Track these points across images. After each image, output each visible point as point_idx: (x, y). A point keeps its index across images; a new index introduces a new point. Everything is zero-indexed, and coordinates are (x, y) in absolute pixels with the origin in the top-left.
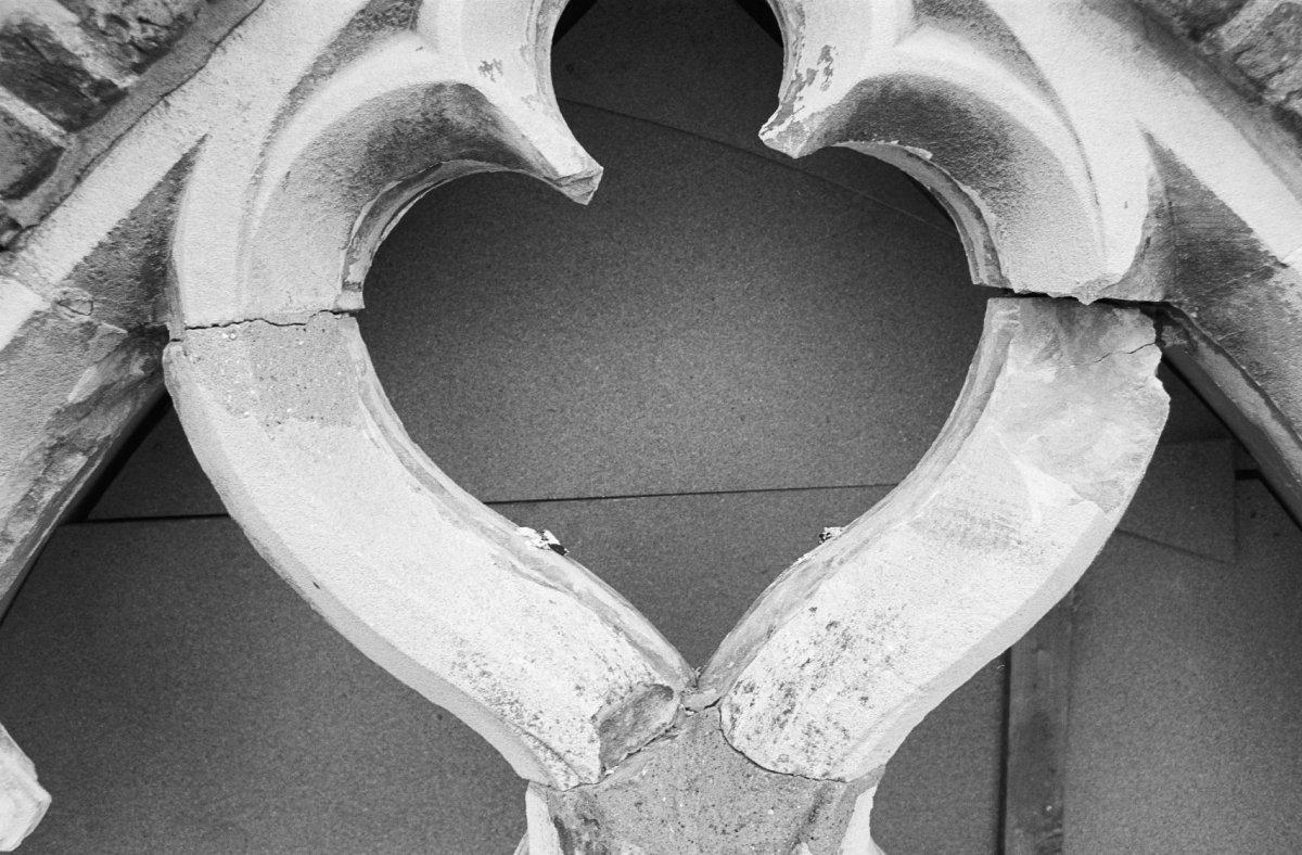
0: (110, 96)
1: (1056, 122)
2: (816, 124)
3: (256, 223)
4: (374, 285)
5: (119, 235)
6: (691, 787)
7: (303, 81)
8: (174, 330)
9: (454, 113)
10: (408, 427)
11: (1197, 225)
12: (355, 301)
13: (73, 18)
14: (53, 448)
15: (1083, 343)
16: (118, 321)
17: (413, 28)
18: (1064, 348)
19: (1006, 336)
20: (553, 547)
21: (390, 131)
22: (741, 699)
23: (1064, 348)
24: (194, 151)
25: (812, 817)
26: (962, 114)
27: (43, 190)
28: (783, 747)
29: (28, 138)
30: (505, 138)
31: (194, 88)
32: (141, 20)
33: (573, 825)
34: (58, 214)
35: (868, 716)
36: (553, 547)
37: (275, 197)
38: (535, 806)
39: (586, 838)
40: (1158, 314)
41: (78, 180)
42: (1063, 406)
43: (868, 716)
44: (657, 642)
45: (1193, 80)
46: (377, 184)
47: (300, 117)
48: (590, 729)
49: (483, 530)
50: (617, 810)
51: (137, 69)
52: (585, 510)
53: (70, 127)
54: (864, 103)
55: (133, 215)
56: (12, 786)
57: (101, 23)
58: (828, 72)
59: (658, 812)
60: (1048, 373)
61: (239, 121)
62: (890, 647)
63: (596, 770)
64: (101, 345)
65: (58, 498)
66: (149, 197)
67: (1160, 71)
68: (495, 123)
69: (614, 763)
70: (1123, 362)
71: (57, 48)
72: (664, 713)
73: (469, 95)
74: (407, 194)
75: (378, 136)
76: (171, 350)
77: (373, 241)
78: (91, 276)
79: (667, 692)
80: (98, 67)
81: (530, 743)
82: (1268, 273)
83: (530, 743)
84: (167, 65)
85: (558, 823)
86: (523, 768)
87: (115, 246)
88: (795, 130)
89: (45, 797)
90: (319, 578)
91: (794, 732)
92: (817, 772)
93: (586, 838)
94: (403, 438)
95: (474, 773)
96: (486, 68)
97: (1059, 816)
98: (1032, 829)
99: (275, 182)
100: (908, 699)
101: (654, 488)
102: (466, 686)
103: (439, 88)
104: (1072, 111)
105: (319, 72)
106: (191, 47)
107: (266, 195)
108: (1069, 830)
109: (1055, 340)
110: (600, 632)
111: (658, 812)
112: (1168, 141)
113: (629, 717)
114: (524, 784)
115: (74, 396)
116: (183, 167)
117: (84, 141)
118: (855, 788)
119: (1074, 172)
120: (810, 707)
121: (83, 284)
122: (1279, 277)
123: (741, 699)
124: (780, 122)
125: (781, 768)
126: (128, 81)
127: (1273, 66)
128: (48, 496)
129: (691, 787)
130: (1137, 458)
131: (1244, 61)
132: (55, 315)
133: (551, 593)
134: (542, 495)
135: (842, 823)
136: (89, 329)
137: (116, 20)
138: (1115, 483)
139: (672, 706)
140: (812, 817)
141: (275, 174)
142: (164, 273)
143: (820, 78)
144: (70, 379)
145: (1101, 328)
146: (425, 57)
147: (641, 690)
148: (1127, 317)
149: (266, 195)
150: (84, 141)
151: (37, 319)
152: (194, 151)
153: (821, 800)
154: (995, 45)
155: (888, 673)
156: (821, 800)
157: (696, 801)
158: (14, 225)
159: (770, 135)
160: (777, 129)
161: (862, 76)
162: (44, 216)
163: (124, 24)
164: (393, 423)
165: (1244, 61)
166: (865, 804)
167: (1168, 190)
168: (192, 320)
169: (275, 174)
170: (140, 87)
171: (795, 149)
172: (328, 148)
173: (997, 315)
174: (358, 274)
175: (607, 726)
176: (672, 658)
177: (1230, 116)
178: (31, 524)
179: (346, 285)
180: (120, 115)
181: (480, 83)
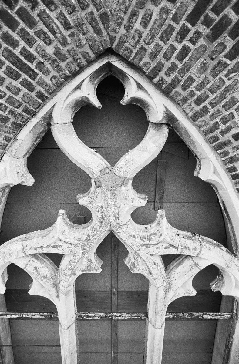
0: (47, 97)
1: (153, 102)
2: (126, 102)
3: (62, 112)
4: (74, 119)
5: (47, 113)
6: (110, 179)
7: (68, 96)
8: (52, 124)
9: (85, 99)
10: (78, 136)
11: (170, 115)
12: (72, 121)
13: (44, 90)
14: (37, 138)
15: (159, 128)
16: (46, 123)
17: (80, 89)
18: (156, 129)
19: (150, 127)
20: (95, 151)
21: (77, 101)
22: (116, 169)
23: (156, 129)
24: (55, 104)
25: (124, 182)
26: (143, 101)
27: (39, 108)
28: (120, 174)
29: (39, 103)
30: (91, 102)
31: (56, 97)
32: (51, 90)
33: (97, 182)
34: (41, 111)
35: (130, 170)
36: (95, 151)
37: (64, 109)
38: (92, 181)
39: (98, 183)
40: (168, 125)
41: (43, 107)
42: (156, 136)
43: (130, 170)
44: (107, 163)
45: (169, 98)
46: (75, 107)
47: (68, 100)
48: (99, 171)
49: (87, 149)
50: (102, 180)
51: (50, 95)
52: (100, 149)
53: (43, 101)
54: (132, 99)
55: (49, 111)
56: (31, 178)
57: (47, 90)
58: (128, 96)
59: (106, 181)
60: (154, 132)
61: (60, 101)
62: (133, 163)
63: (99, 176)
64: (44, 126)
65: (37, 144)
66: (50, 109)
67: (165, 97)
68: (89, 101)
69: (101, 175)
70: (163, 131)
71: (42, 93)
72: (108, 171)
73: (86, 98)
74: (79, 108)
75: (76, 102)
76: (52, 126)
77: (74, 113)
78: (44, 118)
79: (108, 168)
80: (46, 95)
81: (92, 172)
82: (178, 121)
83: (92, 172)
84: (53, 94)
85: (95, 182)
86: (91, 176)
87: (46, 114)
88: (124, 102)
89: (35, 180)
90: (69, 153)
91: (122, 172)
92: (124, 177)
93: (98, 183)
94: (77, 137)
95: (85, 184)
96: (88, 94)
97: (163, 193)
98: (159, 194)
99: (65, 107)
100: (135, 169)
101: (110, 146)
102: (85, 166)
103: (83, 97)
104: (155, 102)
105: (69, 95)
106: (56, 92)
107: (63, 109)
108: (165, 195)
109: (155, 128)
110: (100, 160)
111: (106, 181)
112: (166, 105)
113: (103, 170)
114: (91, 178)
115: (40, 131)
116: (54, 105)
117: (44, 103)
118: (129, 179)
119: (155, 108)
120: (124, 169)
121: (43, 119)
122: (179, 121)
123: (116, 169)
124: (122, 101)
125: (120, 176)
126: (49, 96)
127: (176, 98)
128: (36, 143)
129: (110, 179)
130: (163, 142)
131: (173, 97)
132: (40, 122)
133: (95, 156)
134: (95, 147)
135: (127, 183)
136: (43, 124)
137: (49, 90)
138: (160, 145)
139: (109, 170)
140: (124, 182)
141: (64, 107)
142: (51, 117)
143: (127, 96)
144: (40, 129)
145: (161, 126)
146: (81, 93)
147: (105, 167)
148: (164, 125)
149: (63, 109)
150: (44, 103)
151: (38, 122)
152: (55, 104)
153: (125, 180)
154: (146, 93)
155: (133, 166)
156: (125, 180)
157: (111, 180)
158: (36, 112)
159: (121, 102)
160: (122, 102)
161: (131, 97)
162: (39, 111)
163: (49, 90)
164: (77, 136)
165: (173, 97)
166: (130, 182)
167: (166, 111)
168: (55, 123)
169: (64, 107)
170: (50, 97)
171: (124, 104)
172: (71, 103)
173: (150, 124)
174: (72, 118)
175: (101, 171)
176: (109, 165)
177: (173, 103)
178: (34, 147)
179: (71, 119)
180: (48, 100)
181: (88, 96)
